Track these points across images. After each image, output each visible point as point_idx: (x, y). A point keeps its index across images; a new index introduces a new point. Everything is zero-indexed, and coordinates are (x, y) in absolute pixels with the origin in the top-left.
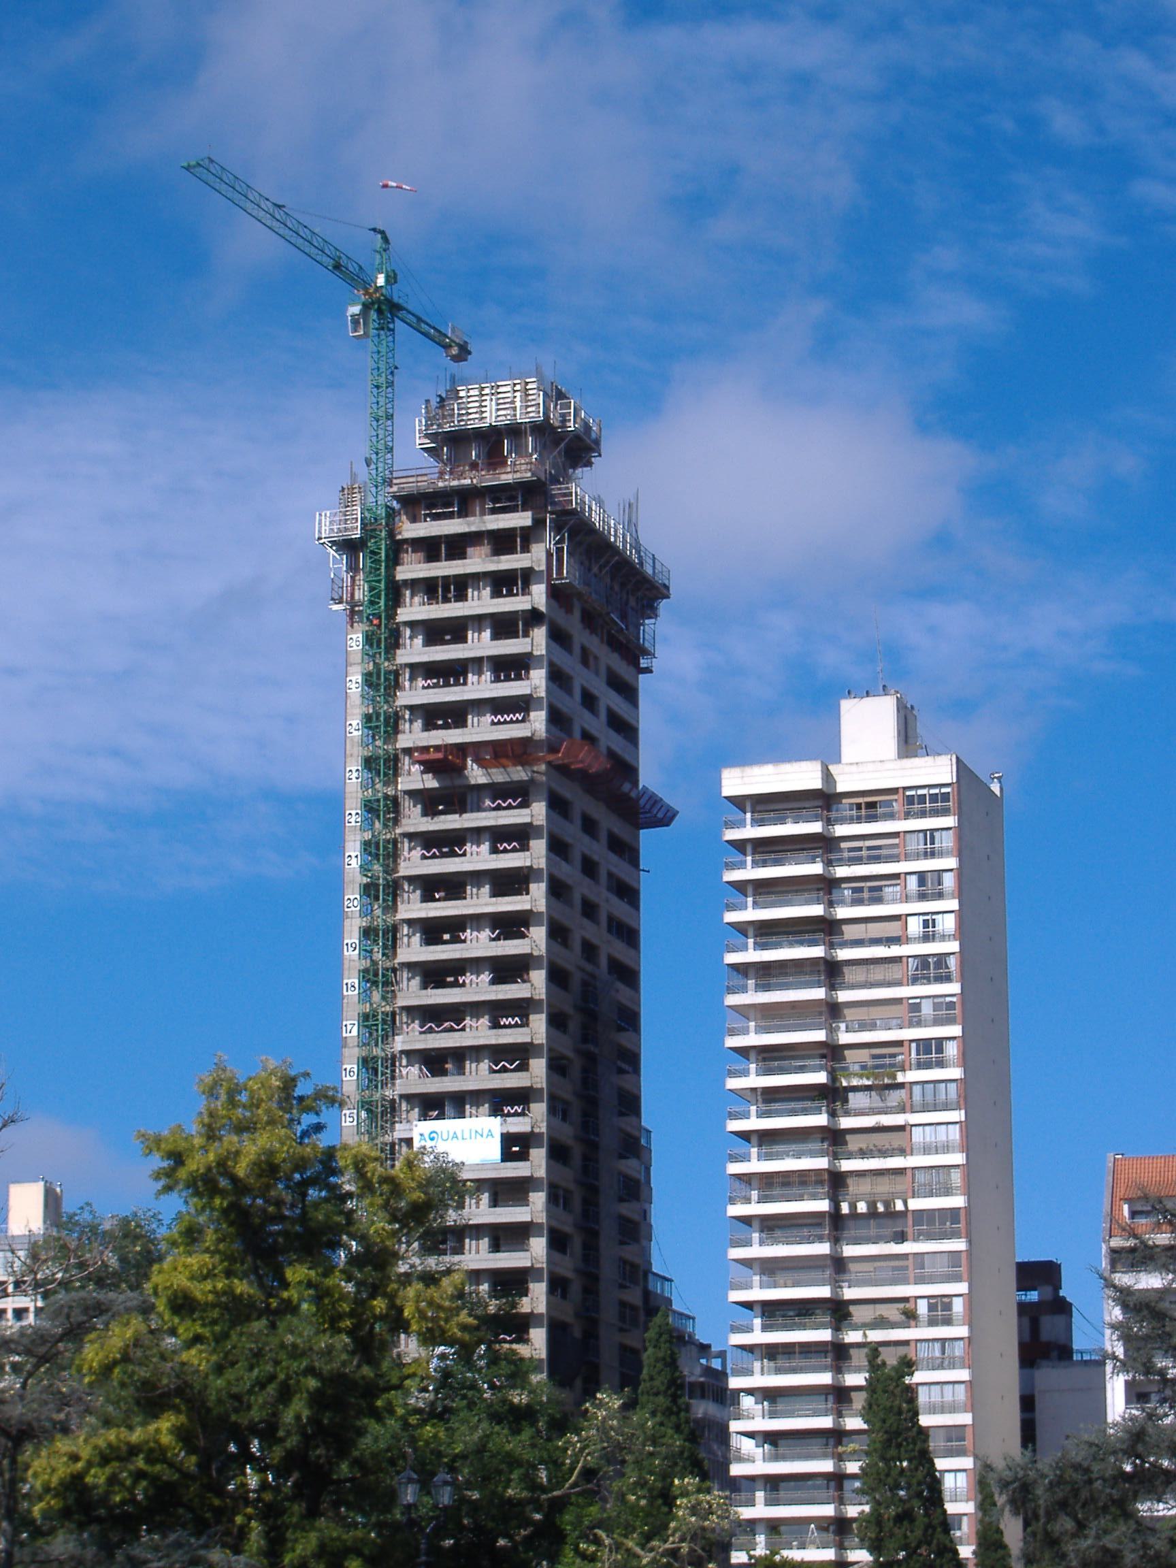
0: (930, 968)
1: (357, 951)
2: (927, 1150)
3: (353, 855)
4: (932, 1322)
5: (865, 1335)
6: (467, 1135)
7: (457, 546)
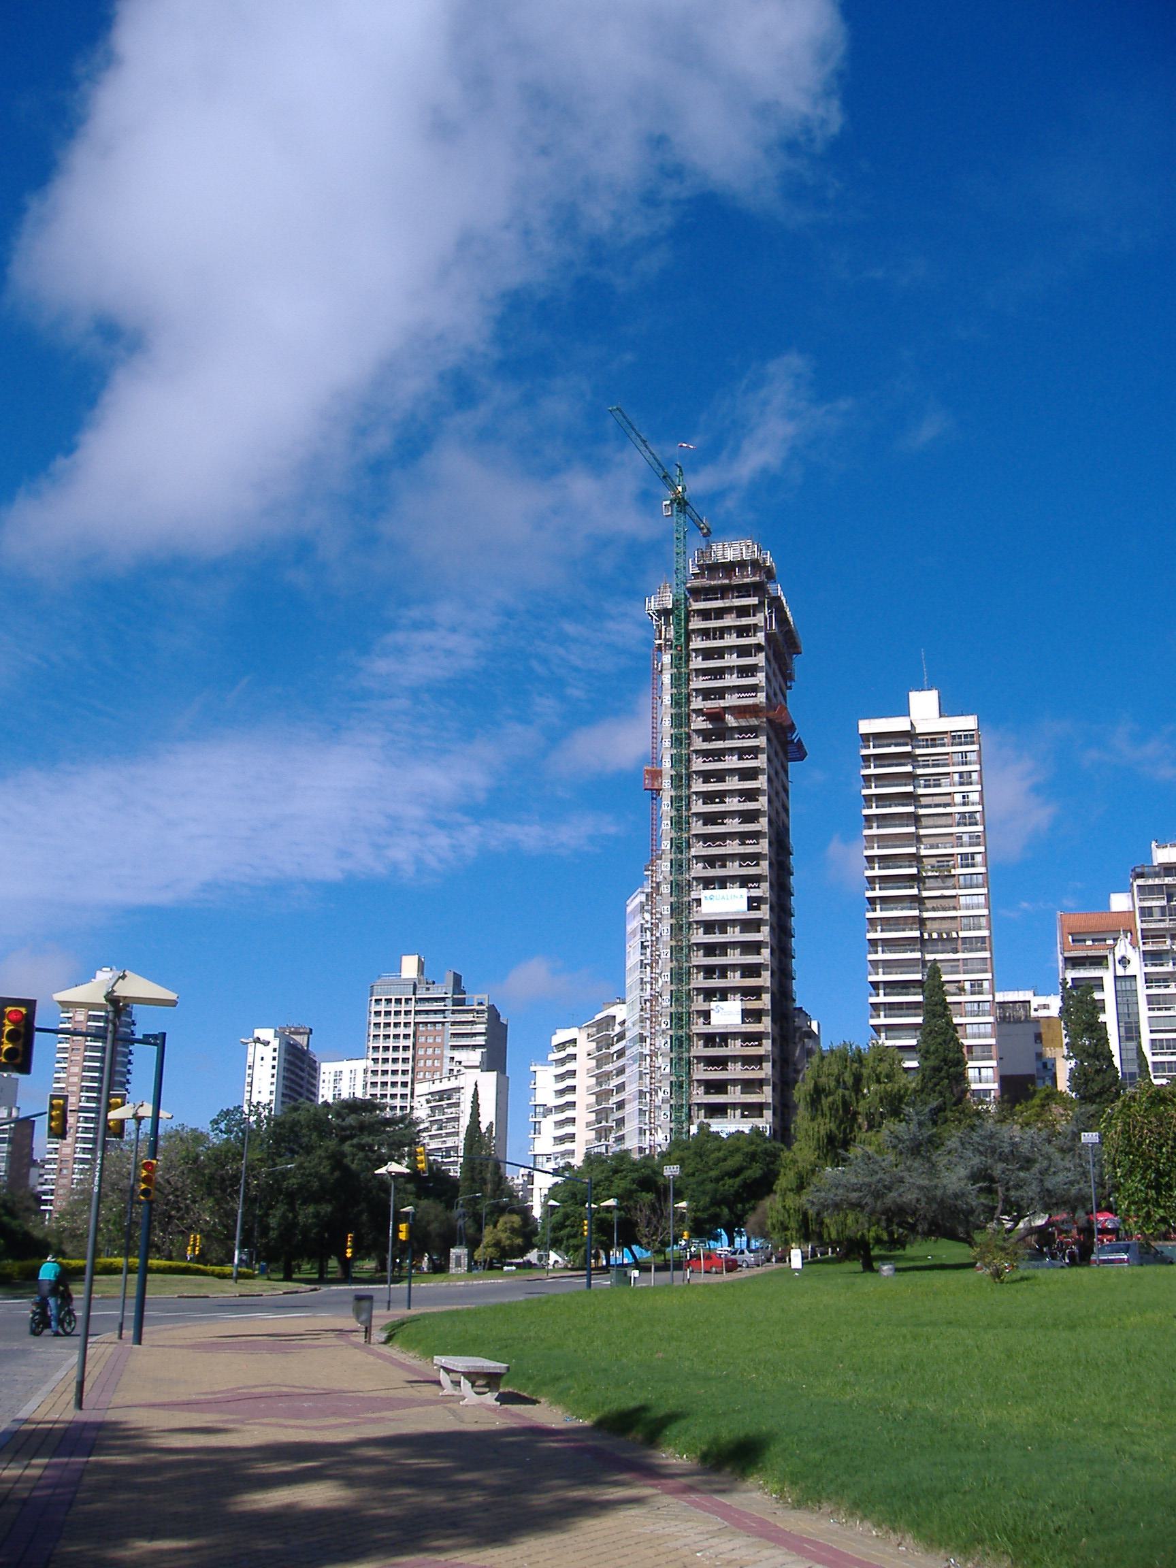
0: (967, 819)
7: (720, 613)
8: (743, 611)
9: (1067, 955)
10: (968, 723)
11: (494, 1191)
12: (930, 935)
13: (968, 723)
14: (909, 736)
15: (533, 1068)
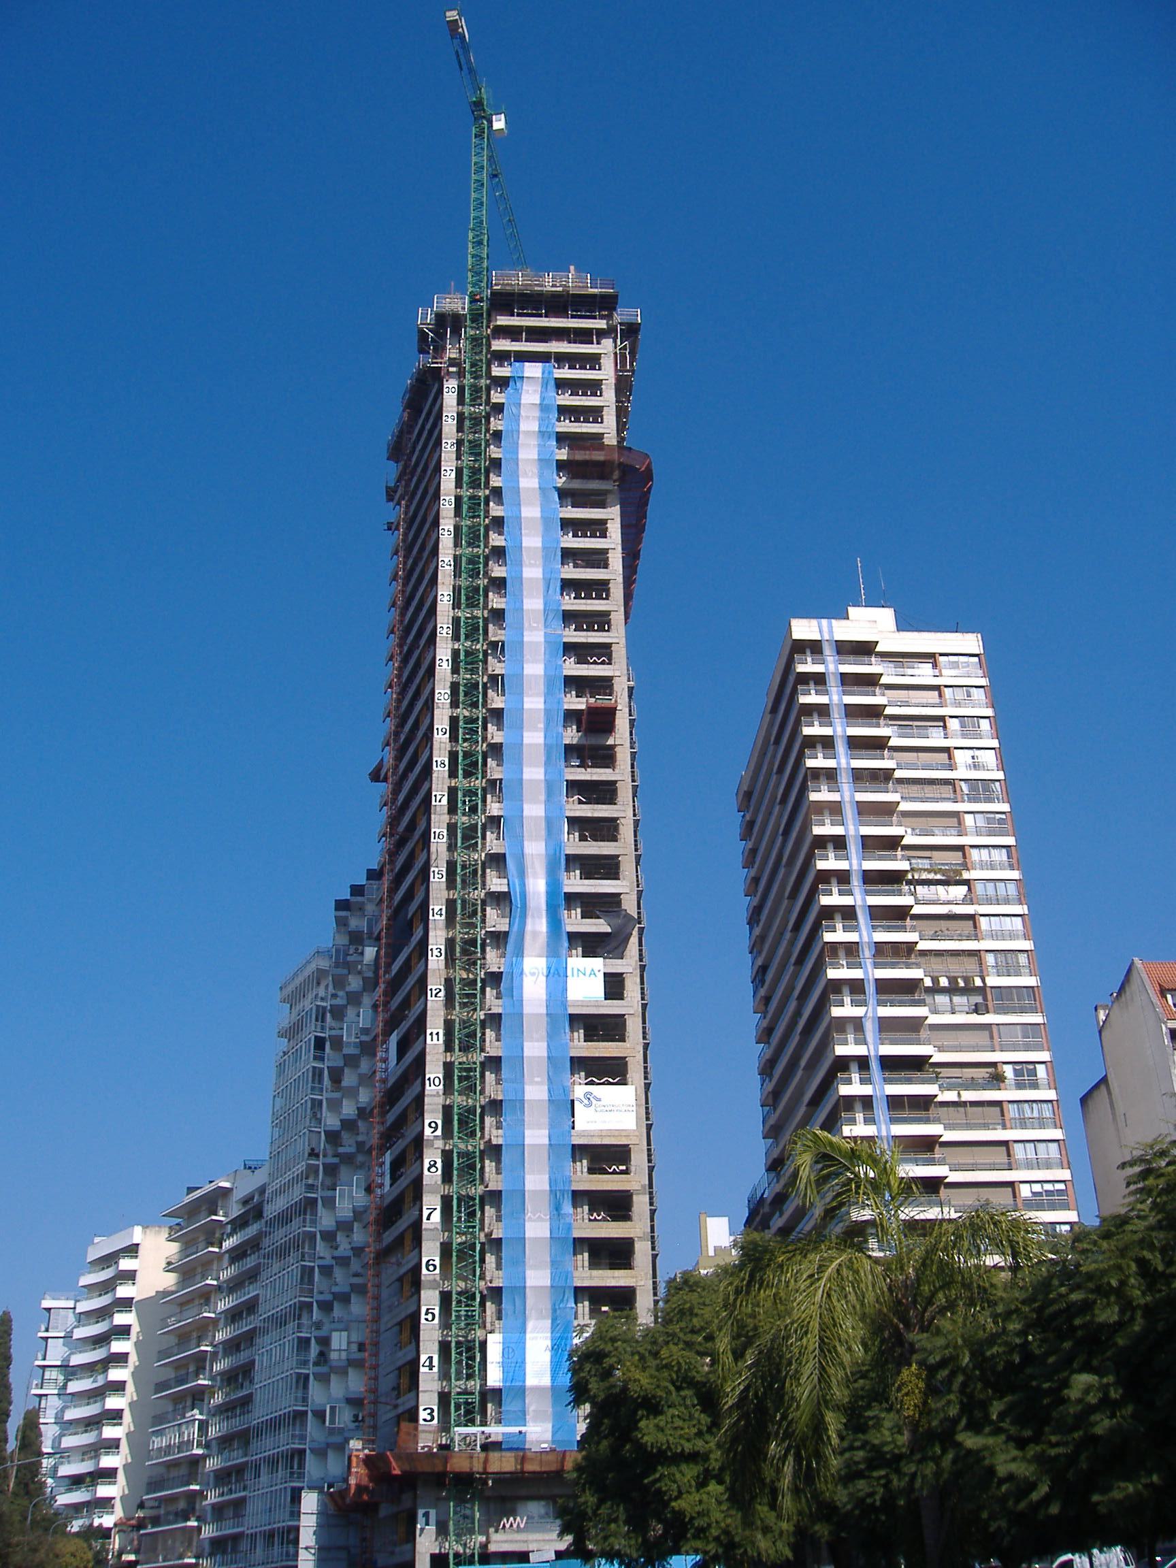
1: (447, 735)
2: (994, 935)
3: (445, 658)
4: (1020, 1086)
5: (959, 1095)
6: (588, 973)
8: (584, 336)
12: (935, 980)
15: (46, 1303)
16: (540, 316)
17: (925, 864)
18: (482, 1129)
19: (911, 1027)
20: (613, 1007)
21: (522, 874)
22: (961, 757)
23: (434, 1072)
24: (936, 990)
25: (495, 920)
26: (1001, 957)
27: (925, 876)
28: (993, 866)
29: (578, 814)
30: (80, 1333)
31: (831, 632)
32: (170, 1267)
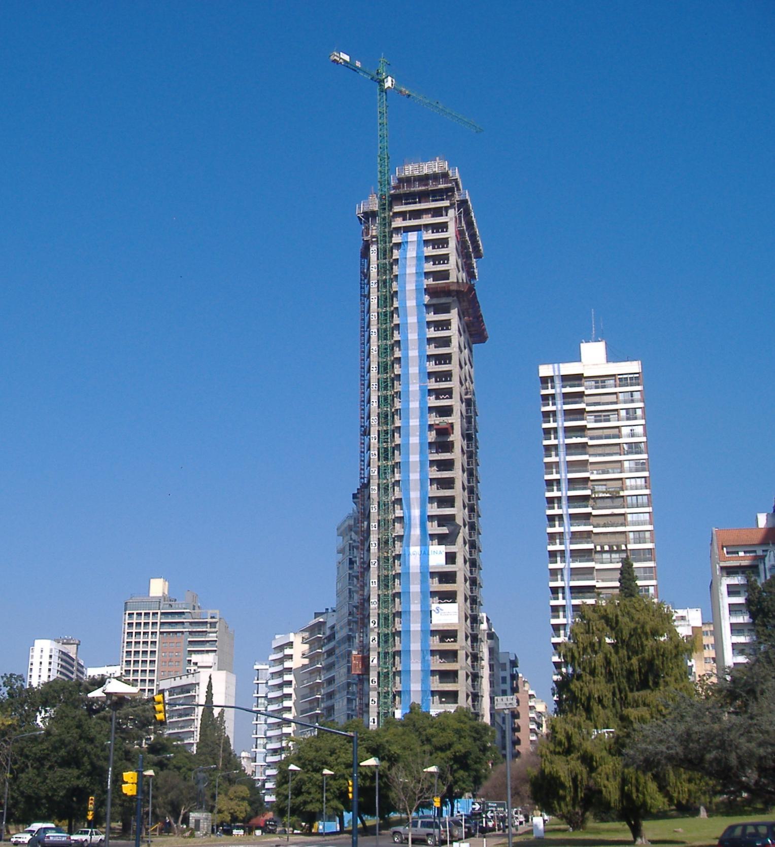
0: (634, 448)
7: (417, 214)
8: (437, 212)
9: (722, 564)
10: (633, 367)
11: (225, 765)
12: (602, 547)
13: (633, 367)
14: (578, 378)
15: (256, 667)
16: (415, 203)
17: (603, 488)
18: (394, 623)
19: (588, 572)
20: (450, 568)
21: (409, 509)
22: (625, 431)
23: (374, 599)
24: (602, 551)
25: (399, 529)
26: (637, 534)
27: (601, 495)
28: (635, 486)
29: (434, 477)
30: (271, 683)
31: (559, 370)
32: (304, 656)
